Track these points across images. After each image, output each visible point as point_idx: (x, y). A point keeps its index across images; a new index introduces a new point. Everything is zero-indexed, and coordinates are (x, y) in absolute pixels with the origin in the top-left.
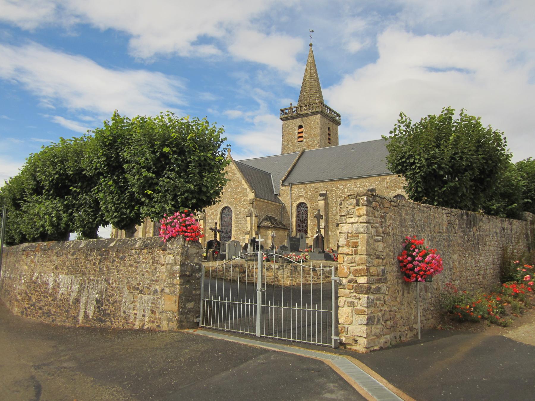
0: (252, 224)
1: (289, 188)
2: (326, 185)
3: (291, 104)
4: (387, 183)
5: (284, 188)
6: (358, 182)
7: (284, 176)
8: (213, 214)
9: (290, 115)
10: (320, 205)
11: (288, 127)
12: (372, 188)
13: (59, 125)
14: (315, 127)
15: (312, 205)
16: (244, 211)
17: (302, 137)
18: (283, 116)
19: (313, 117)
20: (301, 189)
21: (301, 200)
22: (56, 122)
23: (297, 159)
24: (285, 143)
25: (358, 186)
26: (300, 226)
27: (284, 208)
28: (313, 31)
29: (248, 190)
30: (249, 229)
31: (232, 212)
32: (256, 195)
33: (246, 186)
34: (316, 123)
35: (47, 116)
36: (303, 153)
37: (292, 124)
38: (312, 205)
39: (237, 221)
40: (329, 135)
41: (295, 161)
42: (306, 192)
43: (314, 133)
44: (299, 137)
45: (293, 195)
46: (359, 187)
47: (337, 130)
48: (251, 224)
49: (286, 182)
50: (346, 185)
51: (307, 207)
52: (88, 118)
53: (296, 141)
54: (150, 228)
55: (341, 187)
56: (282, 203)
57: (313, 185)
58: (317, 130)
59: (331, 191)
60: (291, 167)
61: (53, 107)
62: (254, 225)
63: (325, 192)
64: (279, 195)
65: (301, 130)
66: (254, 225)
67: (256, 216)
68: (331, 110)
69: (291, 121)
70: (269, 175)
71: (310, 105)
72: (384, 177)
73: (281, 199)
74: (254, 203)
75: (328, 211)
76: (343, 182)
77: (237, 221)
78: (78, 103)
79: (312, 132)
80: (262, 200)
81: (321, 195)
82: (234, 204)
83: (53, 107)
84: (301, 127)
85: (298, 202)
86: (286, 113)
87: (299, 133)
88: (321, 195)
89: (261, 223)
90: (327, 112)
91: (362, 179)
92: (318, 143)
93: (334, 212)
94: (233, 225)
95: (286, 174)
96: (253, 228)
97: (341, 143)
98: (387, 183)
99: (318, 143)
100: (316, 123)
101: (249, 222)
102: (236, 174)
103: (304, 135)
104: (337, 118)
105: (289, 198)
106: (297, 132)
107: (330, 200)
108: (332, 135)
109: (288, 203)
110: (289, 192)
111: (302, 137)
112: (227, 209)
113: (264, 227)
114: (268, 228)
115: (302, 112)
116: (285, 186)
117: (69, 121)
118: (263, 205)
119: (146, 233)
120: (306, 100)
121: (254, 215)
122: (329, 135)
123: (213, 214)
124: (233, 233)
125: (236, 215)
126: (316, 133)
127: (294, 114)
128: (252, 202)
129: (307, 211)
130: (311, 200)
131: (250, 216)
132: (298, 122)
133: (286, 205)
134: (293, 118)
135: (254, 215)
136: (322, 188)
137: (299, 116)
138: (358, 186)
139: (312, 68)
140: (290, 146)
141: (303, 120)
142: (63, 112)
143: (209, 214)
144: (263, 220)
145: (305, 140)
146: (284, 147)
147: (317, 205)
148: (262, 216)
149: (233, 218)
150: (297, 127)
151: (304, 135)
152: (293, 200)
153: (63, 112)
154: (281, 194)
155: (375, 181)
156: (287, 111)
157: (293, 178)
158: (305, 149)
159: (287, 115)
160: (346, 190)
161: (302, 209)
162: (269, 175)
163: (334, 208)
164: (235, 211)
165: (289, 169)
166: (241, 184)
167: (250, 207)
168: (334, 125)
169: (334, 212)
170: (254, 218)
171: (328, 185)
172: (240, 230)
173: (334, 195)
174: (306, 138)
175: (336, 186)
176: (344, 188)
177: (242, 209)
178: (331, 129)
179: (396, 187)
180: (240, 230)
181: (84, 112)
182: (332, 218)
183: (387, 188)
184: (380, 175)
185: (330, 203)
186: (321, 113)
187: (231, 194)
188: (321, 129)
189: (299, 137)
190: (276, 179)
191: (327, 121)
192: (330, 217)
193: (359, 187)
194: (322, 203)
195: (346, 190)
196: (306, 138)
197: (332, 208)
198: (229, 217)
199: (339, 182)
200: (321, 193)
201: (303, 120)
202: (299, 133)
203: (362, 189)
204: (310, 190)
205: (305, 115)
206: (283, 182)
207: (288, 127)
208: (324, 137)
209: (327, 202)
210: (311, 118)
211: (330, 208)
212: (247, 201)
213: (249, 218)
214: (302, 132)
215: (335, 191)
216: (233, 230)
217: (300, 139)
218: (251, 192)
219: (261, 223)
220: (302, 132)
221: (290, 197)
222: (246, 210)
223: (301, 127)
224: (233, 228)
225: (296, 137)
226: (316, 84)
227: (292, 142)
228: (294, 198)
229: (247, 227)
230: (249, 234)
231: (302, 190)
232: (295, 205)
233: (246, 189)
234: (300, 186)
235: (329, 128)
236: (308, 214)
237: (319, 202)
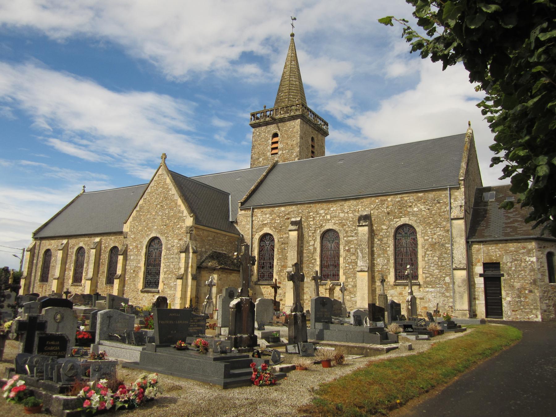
0: (188, 263)
1: (249, 213)
2: (301, 208)
3: (265, 107)
4: (387, 207)
5: (243, 212)
6: (347, 204)
7: (245, 197)
8: (137, 247)
9: (262, 120)
10: (291, 237)
11: (259, 136)
12: (365, 213)
13: (53, 147)
14: (294, 136)
15: (281, 238)
16: (178, 243)
17: (276, 148)
18: (253, 122)
19: (292, 123)
20: (266, 214)
21: (266, 230)
22: (51, 144)
23: (264, 174)
24: (256, 156)
25: (346, 211)
26: (263, 268)
27: (241, 240)
28: (295, 19)
29: (186, 213)
30: (182, 271)
31: (162, 245)
32: (197, 220)
33: (183, 208)
34: (295, 130)
35: (40, 138)
36: (274, 166)
37: (265, 132)
38: (281, 238)
39: (168, 259)
40: (313, 147)
41: (262, 176)
42: (273, 219)
43: (292, 143)
44: (273, 149)
45: (255, 222)
46: (347, 213)
47: (323, 142)
48: (187, 263)
49: (246, 205)
50: (329, 209)
51: (273, 240)
52: (85, 142)
53: (269, 154)
54: (70, 264)
55: (322, 212)
56: (239, 234)
57: (283, 209)
58: (297, 140)
59: (307, 218)
60: (256, 184)
61: (48, 127)
62: (190, 265)
63: (298, 219)
64: (237, 223)
65: (275, 139)
66: (190, 265)
67: (194, 252)
68: (316, 116)
69: (263, 128)
70: (226, 195)
71: (287, 108)
72: (384, 198)
73: (238, 228)
74: (194, 232)
75: (302, 247)
76: (325, 206)
77: (168, 259)
78: (78, 125)
79: (289, 142)
80: (205, 228)
81: (293, 223)
82: (165, 234)
83: (48, 127)
84: (275, 135)
85: (261, 233)
86: (258, 118)
87: (273, 143)
88: (293, 223)
89: (203, 262)
90: (310, 117)
91: (352, 201)
92: (297, 156)
93: (311, 248)
94: (162, 265)
95: (248, 193)
96: (190, 270)
97: (328, 154)
98: (387, 207)
99: (297, 156)
100: (295, 130)
101: (183, 261)
102: (170, 189)
103: (279, 145)
104: (324, 127)
105: (249, 226)
106: (270, 142)
107: (305, 231)
108: (316, 147)
109: (248, 235)
110: (250, 219)
111: (276, 148)
112: (156, 241)
113: (207, 267)
114: (213, 270)
115: (278, 116)
116: (245, 210)
117: (65, 143)
118: (208, 236)
119: (65, 271)
120: (283, 102)
121: (191, 251)
122: (313, 147)
123: (137, 247)
124: (162, 276)
125: (168, 249)
126: (294, 143)
127: (268, 119)
128: (190, 230)
129: (273, 246)
130: (279, 229)
131: (186, 251)
132: (273, 128)
133: (245, 237)
134: (267, 124)
135: (191, 251)
136: (295, 213)
137: (274, 121)
138: (346, 211)
139: (293, 63)
140: (261, 159)
141: (278, 127)
142: (58, 133)
143: (131, 248)
144: (207, 258)
145: (280, 153)
146: (254, 161)
147: (288, 238)
148: (206, 252)
149: (163, 253)
150: (271, 136)
151: (279, 145)
152: (254, 230)
153: (58, 133)
154: (238, 221)
155: (371, 204)
156: (259, 115)
157: (257, 199)
158: (277, 162)
159: (260, 121)
160: (329, 217)
161: (267, 243)
162: (226, 195)
163: (312, 243)
164: (167, 244)
165: (253, 187)
166: (176, 204)
167: (187, 239)
168: (320, 136)
169: (311, 248)
170: (191, 254)
171: (304, 209)
172: (172, 272)
173: (312, 223)
174: (282, 149)
175: (314, 210)
176: (326, 214)
177: (176, 241)
178: (315, 139)
179: (401, 213)
180: (172, 272)
181: (82, 135)
182: (308, 257)
183: (388, 213)
184: (377, 196)
185: (306, 235)
186: (302, 117)
187: (162, 219)
188: (301, 138)
189: (273, 149)
190: (234, 202)
191: (310, 130)
192: (305, 255)
193: (347, 213)
194: (294, 235)
195: (329, 217)
196: (282, 149)
197: (308, 242)
198: (158, 252)
199: (318, 206)
200: (293, 220)
201: (278, 127)
202: (273, 143)
203: (351, 215)
204: (279, 217)
205: (282, 120)
206: (243, 204)
207: (259, 136)
208: (305, 149)
209: (30, 282)
210: (288, 124)
211: (305, 243)
212: (183, 230)
213: (183, 255)
214: (277, 142)
215: (314, 217)
216: (161, 271)
217: (274, 151)
218: (188, 216)
219: (203, 262)
220: (277, 142)
221: (251, 226)
222: (181, 242)
223: (275, 135)
224: (162, 268)
225: (269, 148)
226: (297, 83)
227: (264, 154)
228: (256, 227)
229: (179, 268)
230: (181, 278)
231: (268, 216)
232: (257, 237)
233: (183, 213)
234: (265, 210)
235: (313, 139)
236: (275, 250)
237: (291, 233)
